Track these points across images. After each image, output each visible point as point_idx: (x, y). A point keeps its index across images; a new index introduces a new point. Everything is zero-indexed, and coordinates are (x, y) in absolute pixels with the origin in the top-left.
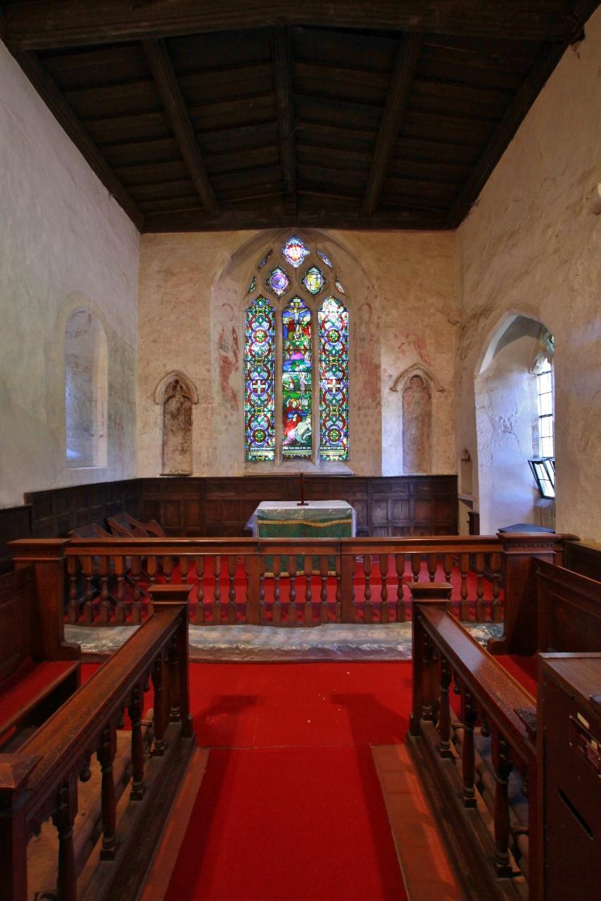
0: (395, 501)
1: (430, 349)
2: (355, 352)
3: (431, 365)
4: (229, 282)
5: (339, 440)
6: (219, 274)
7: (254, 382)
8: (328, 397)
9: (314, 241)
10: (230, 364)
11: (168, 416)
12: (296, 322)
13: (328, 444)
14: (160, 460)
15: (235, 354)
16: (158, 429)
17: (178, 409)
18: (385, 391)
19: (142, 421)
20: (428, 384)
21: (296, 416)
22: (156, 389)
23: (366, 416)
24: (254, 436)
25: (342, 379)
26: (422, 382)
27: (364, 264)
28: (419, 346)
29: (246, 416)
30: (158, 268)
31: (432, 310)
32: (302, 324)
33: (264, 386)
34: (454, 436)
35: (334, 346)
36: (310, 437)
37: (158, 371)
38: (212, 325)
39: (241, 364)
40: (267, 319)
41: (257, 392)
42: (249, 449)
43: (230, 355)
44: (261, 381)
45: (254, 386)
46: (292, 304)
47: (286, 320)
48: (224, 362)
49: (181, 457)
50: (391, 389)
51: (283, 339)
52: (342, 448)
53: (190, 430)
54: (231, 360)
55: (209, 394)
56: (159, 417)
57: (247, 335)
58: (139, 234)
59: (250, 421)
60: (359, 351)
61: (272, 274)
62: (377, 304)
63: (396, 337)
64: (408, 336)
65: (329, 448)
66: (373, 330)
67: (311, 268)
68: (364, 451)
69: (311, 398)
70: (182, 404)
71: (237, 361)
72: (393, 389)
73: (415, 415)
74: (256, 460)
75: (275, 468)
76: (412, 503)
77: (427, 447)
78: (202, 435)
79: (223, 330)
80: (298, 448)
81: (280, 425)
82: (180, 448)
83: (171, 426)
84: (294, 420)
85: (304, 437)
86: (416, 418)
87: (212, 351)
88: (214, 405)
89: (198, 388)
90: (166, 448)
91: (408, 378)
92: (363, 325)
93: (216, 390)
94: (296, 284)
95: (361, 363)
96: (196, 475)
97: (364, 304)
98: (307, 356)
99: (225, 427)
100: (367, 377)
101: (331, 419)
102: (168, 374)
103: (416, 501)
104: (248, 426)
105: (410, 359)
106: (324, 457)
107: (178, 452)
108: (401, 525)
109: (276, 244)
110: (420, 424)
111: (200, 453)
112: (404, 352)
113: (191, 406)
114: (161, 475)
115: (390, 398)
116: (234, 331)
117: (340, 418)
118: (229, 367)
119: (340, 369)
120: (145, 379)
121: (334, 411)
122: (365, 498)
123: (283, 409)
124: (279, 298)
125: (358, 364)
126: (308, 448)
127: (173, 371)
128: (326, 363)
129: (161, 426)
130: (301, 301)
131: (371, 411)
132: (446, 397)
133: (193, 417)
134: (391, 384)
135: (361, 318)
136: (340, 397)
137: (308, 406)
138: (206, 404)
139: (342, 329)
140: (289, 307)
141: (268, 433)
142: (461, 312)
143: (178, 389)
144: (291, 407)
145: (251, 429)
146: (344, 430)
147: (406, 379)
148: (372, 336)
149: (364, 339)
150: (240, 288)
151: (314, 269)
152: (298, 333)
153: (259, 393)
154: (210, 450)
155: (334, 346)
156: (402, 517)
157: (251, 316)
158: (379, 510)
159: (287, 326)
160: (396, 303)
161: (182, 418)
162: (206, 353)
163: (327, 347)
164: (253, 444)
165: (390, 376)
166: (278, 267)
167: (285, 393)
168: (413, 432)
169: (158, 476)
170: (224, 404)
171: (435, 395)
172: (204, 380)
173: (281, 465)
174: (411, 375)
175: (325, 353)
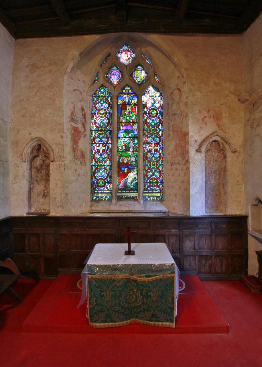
0: (201, 236)
1: (225, 121)
2: (169, 123)
3: (226, 133)
4: (79, 75)
5: (157, 186)
6: (71, 65)
7: (98, 145)
8: (149, 155)
9: (139, 46)
10: (80, 132)
11: (34, 170)
12: (126, 103)
13: (149, 189)
14: (26, 203)
15: (84, 126)
16: (25, 180)
17: (41, 165)
18: (192, 152)
19: (13, 174)
20: (224, 147)
21: (126, 169)
22: (23, 151)
23: (177, 169)
24: (97, 183)
25: (159, 143)
26: (219, 146)
27: (176, 59)
28: (217, 119)
29: (92, 169)
30: (27, 63)
31: (227, 92)
32: (131, 105)
33: (104, 148)
34: (244, 185)
35: (153, 120)
36: (137, 183)
37: (25, 138)
38: (65, 103)
39: (88, 133)
40: (107, 101)
41: (99, 152)
42: (94, 192)
43: (80, 126)
44: (103, 144)
45: (98, 148)
46: (124, 91)
47: (120, 102)
48: (74, 131)
49: (43, 200)
50: (197, 150)
51: (118, 115)
52: (159, 191)
53: (49, 180)
54: (80, 130)
55: (62, 155)
56: (26, 172)
57: (93, 112)
58: (14, 39)
59: (95, 172)
60: (171, 123)
61: (110, 71)
62: (185, 88)
63: (200, 112)
64: (209, 111)
65: (150, 191)
66: (183, 107)
67: (137, 66)
68: (175, 195)
69: (137, 156)
70: (44, 161)
71: (85, 130)
72: (198, 151)
73: (214, 170)
74: (99, 200)
75: (112, 206)
76: (213, 237)
77: (223, 193)
78: (57, 185)
79: (74, 108)
80: (128, 191)
81: (115, 176)
82: (42, 194)
83: (36, 177)
84: (126, 171)
85: (132, 184)
86: (215, 172)
87: (65, 123)
88: (65, 162)
89: (54, 150)
90: (32, 194)
91: (209, 142)
92: (175, 104)
93: (68, 151)
94: (127, 76)
95: (173, 131)
96: (53, 214)
97: (175, 90)
98: (135, 127)
99: (76, 178)
100: (178, 142)
101: (151, 171)
102: (32, 140)
103: (216, 236)
104: (93, 176)
105: (210, 128)
106: (147, 197)
107: (41, 196)
108: (205, 254)
109: (113, 49)
110: (218, 176)
111: (55, 198)
112: (206, 123)
113: (49, 163)
114: (27, 214)
115: (196, 157)
116: (83, 109)
117: (158, 170)
118: (78, 135)
119: (158, 136)
120: (15, 144)
121: (154, 165)
122: (178, 233)
123: (118, 164)
124: (115, 87)
125: (171, 133)
126: (135, 191)
127: (36, 138)
128: (148, 132)
129: (28, 178)
130: (130, 89)
131: (181, 166)
132: (238, 157)
133: (51, 171)
134: (196, 147)
135: (173, 99)
136: (157, 155)
137: (135, 162)
138: (60, 162)
139: (107, 178)
140: (122, 93)
141: (107, 181)
142: (250, 92)
143: (41, 150)
144: (123, 162)
145: (95, 178)
146: (161, 179)
147: (207, 143)
148: (182, 112)
149: (175, 115)
150: (88, 79)
151: (139, 67)
152: (128, 111)
153: (101, 153)
154: (63, 196)
155: (153, 120)
156: (206, 247)
157: (95, 99)
158: (188, 242)
159: (120, 106)
160: (199, 87)
161: (44, 172)
162: (60, 124)
163: (149, 121)
164: (97, 189)
165: (196, 141)
166: (114, 66)
167: (119, 152)
168: (212, 182)
169: (25, 215)
170: (74, 162)
171: (229, 155)
172: (58, 144)
173: (116, 204)
174: (211, 140)
175: (147, 125)
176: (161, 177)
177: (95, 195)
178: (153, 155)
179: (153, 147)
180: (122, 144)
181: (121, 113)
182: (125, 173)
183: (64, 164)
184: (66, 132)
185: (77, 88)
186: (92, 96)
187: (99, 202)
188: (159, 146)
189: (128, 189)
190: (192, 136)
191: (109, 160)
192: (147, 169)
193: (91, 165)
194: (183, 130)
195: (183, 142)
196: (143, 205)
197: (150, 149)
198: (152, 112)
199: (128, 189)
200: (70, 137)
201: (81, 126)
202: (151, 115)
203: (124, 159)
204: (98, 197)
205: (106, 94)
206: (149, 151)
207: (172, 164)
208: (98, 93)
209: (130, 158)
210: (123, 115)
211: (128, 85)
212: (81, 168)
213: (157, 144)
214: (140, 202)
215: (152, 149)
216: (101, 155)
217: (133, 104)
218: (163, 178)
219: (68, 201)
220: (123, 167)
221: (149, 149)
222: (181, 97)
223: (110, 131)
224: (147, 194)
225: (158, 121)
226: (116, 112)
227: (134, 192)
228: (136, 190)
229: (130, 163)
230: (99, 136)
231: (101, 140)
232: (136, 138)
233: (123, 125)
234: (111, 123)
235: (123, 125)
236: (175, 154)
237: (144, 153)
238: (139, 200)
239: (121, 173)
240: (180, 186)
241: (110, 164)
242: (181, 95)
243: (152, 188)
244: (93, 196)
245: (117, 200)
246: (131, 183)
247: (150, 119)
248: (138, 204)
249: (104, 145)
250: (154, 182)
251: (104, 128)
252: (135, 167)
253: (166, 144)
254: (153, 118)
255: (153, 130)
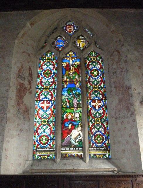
2: (110, 81)
5: (102, 142)
7: (42, 102)
10: (26, 88)
12: (70, 65)
13: (94, 146)
15: (30, 83)
21: (70, 125)
25: (102, 99)
32: (74, 66)
33: (48, 105)
36: (81, 140)
38: (13, 62)
40: (52, 64)
42: (36, 150)
43: (26, 83)
44: (47, 101)
46: (68, 55)
47: (64, 64)
48: (20, 86)
52: (105, 149)
60: (113, 80)
62: (124, 49)
65: (95, 149)
71: (31, 88)
79: (22, 66)
80: (73, 149)
84: (70, 128)
85: (77, 141)
92: (115, 64)
93: (12, 104)
95: (115, 87)
97: (114, 52)
101: (95, 127)
116: (30, 69)
117: (102, 126)
118: (24, 91)
119: (100, 93)
121: (98, 121)
123: (62, 120)
125: (113, 89)
136: (101, 111)
138: (3, 115)
144: (67, 118)
145: (38, 135)
146: (106, 135)
152: (72, 71)
155: (95, 79)
157: (42, 62)
165: (139, 93)
170: (18, 116)
175: (90, 83)
176: (106, 133)
177: (37, 154)
178: (97, 111)
179: (97, 104)
180: (66, 101)
181: (65, 73)
182: (70, 130)
183: (7, 117)
184: (12, 87)
185: (26, 51)
186: (40, 59)
187: (41, 161)
188: (102, 102)
189: (72, 146)
190: (135, 89)
191: (53, 116)
192: (91, 125)
193: (35, 122)
194: (125, 85)
195: (126, 95)
196: (88, 164)
197: (93, 105)
198: (98, 137)
199: (72, 146)
200: (15, 91)
201: (28, 83)
202: (93, 75)
203: (68, 115)
204: (40, 156)
205: (51, 57)
206: (94, 143)
207: (116, 119)
208: (45, 57)
209: (74, 114)
210: (68, 75)
211: (71, 51)
212: (24, 124)
213: (100, 101)
214: (86, 160)
215: (95, 105)
216: (45, 112)
217: (76, 65)
218: (109, 134)
219: (7, 158)
220: (67, 123)
221: (93, 105)
222: (120, 57)
223: (54, 89)
224: (94, 152)
225: (99, 79)
226: (61, 72)
227: (78, 150)
228: (81, 147)
229: (74, 119)
230: (44, 94)
231: (46, 97)
232: (80, 95)
233: (67, 83)
234: (56, 82)
235: (67, 83)
236: (119, 108)
237: (88, 110)
238: (84, 158)
239: (65, 129)
240: (127, 141)
241: (54, 121)
242: (120, 55)
243: (97, 144)
244: (35, 154)
245: (61, 159)
246: (76, 140)
247: (93, 78)
248: (84, 162)
249: (49, 102)
250: (100, 138)
251: (49, 87)
252: (79, 123)
253: (109, 100)
254: (95, 78)
255: (94, 59)
